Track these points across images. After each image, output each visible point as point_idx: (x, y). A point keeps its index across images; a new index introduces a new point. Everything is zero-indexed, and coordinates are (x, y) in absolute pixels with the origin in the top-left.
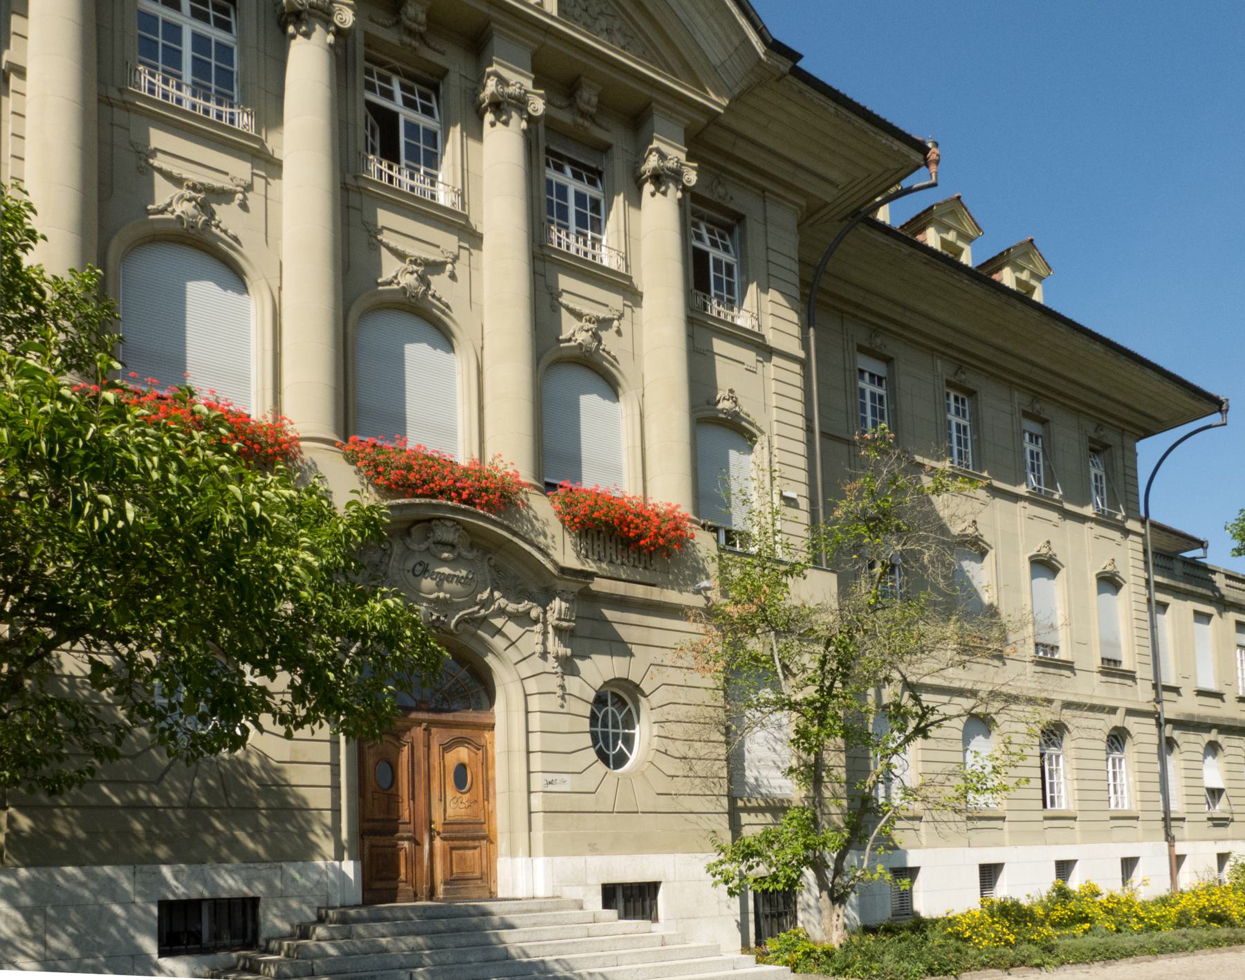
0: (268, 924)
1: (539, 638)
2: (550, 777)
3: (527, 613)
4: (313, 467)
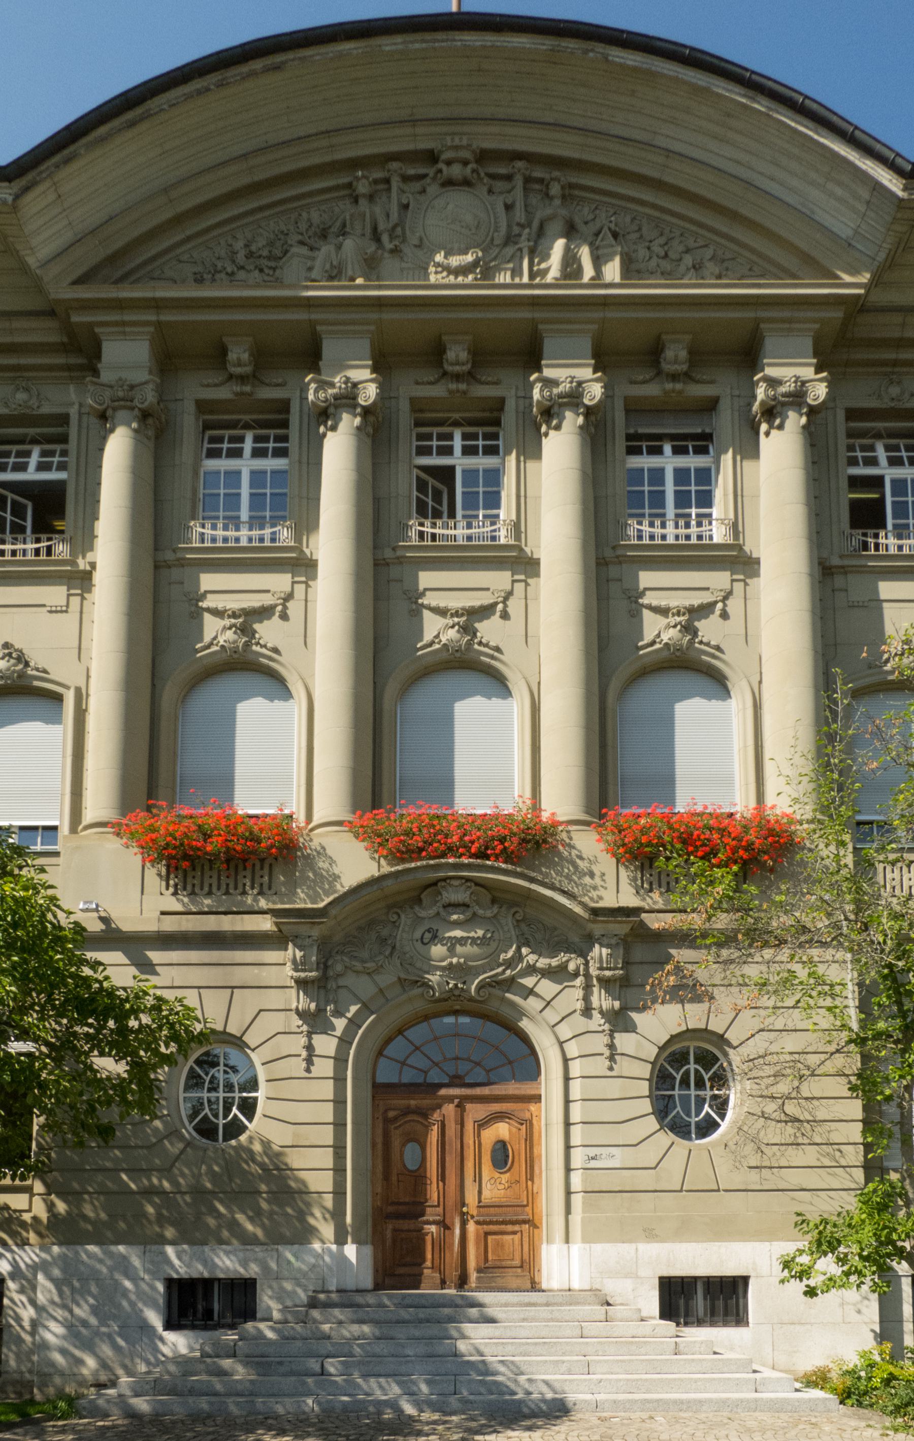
0: (263, 1305)
1: (580, 993)
2: (592, 1152)
3: (563, 967)
4: (322, 852)
